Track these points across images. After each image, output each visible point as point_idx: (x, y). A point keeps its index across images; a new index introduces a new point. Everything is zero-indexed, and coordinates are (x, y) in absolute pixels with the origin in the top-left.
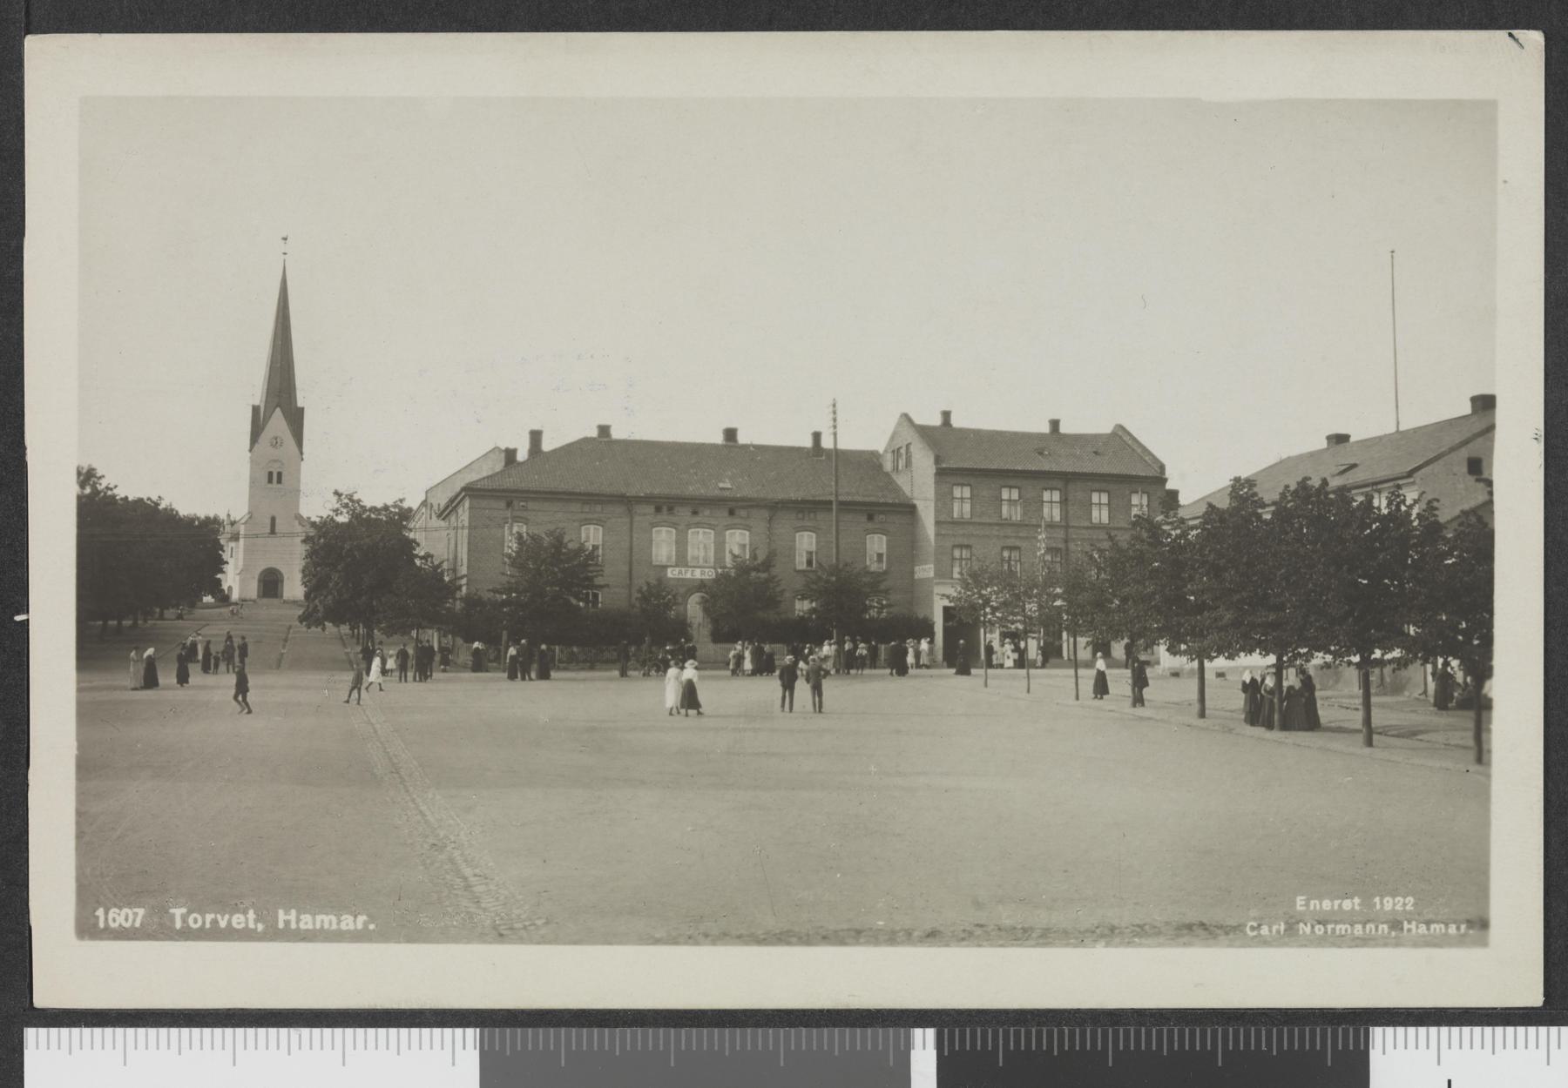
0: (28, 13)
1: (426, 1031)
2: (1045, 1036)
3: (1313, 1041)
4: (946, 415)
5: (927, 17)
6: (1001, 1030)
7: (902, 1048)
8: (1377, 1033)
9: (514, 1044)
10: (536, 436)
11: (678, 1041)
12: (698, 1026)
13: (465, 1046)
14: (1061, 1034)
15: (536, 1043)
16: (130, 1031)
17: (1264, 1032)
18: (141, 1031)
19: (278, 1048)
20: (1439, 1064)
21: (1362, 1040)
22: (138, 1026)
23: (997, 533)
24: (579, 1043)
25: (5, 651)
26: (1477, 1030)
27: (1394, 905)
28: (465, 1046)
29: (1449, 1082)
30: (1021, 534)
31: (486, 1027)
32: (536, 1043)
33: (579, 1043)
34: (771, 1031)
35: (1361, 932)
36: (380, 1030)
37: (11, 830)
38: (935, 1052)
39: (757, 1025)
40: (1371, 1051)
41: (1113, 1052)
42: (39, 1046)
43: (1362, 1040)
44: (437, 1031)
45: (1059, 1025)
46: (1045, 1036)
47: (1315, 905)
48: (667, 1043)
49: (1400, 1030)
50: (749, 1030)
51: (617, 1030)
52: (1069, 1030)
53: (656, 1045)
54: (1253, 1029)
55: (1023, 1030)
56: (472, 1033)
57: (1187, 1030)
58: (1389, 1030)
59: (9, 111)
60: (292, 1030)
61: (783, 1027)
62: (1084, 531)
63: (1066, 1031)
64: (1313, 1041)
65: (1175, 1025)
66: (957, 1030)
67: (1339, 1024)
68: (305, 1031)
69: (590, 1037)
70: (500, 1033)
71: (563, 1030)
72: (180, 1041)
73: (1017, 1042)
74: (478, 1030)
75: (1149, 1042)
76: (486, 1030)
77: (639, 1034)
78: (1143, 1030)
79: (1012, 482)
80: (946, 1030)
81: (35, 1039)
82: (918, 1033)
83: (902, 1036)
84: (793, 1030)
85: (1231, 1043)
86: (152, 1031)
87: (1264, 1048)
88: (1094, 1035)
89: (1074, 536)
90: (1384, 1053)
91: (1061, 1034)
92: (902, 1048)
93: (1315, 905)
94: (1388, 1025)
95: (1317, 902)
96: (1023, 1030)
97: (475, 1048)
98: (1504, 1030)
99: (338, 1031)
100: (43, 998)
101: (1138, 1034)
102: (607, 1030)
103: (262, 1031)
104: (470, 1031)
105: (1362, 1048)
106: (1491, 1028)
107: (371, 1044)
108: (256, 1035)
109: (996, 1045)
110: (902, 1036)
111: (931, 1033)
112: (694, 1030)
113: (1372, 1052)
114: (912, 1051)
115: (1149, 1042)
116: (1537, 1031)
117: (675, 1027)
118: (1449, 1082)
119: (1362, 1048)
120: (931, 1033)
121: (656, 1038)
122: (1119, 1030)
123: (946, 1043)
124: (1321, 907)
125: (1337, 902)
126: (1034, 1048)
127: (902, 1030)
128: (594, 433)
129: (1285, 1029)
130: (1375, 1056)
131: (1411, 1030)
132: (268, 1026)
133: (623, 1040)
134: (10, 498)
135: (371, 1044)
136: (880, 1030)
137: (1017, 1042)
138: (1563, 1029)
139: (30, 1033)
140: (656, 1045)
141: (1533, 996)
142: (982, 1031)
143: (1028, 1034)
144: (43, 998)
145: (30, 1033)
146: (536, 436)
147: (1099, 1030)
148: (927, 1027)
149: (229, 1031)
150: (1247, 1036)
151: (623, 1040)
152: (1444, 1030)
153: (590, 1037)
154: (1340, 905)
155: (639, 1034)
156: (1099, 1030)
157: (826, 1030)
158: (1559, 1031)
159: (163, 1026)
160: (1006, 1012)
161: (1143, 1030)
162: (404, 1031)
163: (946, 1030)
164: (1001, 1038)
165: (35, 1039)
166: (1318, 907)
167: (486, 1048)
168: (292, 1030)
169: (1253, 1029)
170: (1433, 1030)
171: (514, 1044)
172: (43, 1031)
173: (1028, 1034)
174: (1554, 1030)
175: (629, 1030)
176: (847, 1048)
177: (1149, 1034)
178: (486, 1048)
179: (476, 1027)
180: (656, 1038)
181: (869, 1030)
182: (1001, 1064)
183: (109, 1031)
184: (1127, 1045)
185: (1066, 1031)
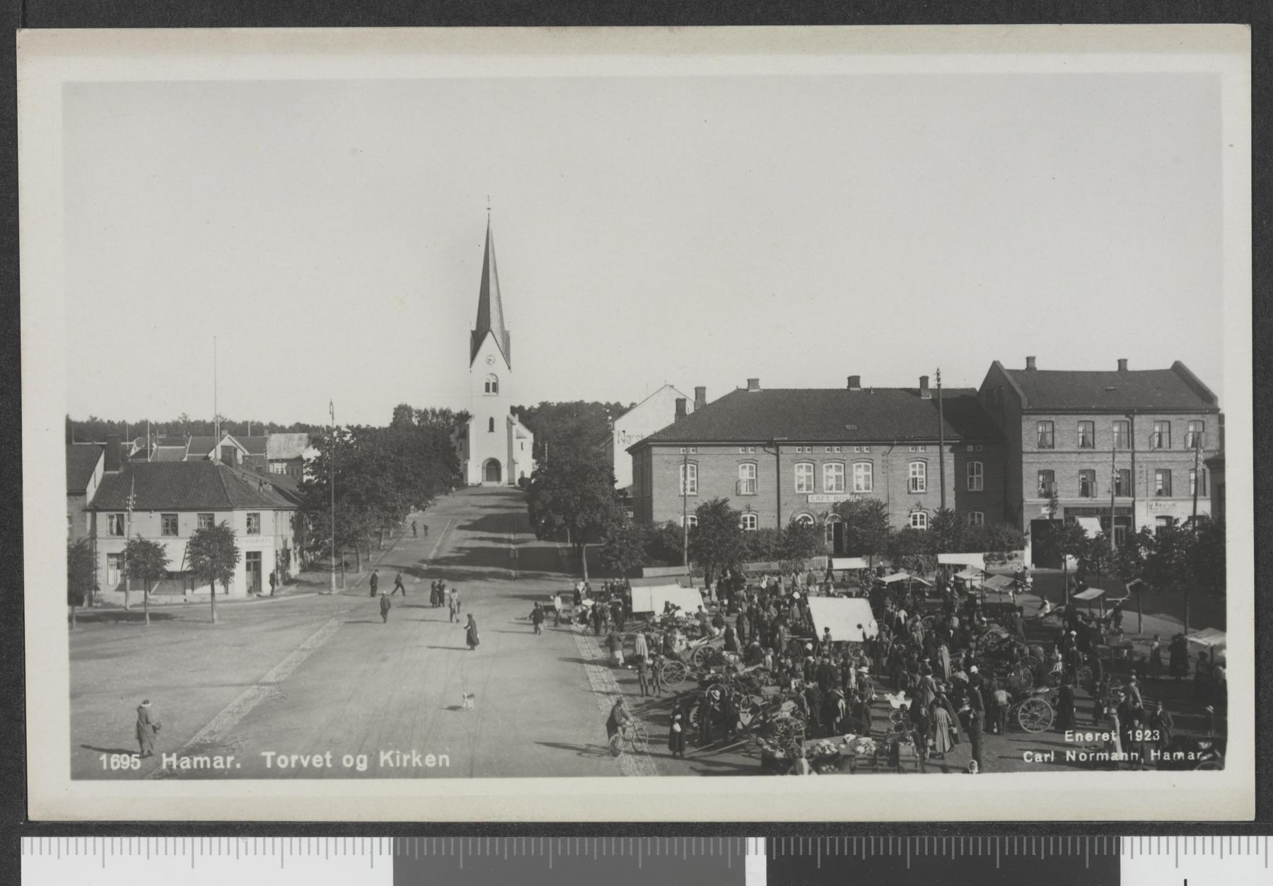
0: (24, 8)
1: (349, 840)
2: (855, 844)
3: (806, 847)
4: (1030, 360)
5: (759, 11)
6: (819, 839)
7: (739, 854)
8: (1126, 841)
9: (600, 851)
10: (700, 392)
11: (466, 847)
12: (572, 836)
13: (382, 851)
14: (868, 842)
15: (663, 850)
16: (108, 840)
17: (1034, 841)
18: (117, 839)
19: (50, 853)
20: (104, 867)
21: (399, 847)
22: (115, 836)
23: (1074, 460)
24: (475, 849)
25: (5, 529)
26: (1208, 839)
27: (1144, 736)
28: (382, 851)
29: (1186, 881)
30: (1095, 460)
31: (398, 836)
32: (663, 850)
33: (475, 849)
34: (631, 839)
35: (1169, 759)
36: (34, 838)
37: (11, 675)
38: (765, 856)
39: (620, 835)
40: (1122, 856)
41: (911, 857)
42: (34, 852)
43: (399, 847)
44: (358, 840)
45: (866, 834)
46: (855, 844)
47: (1079, 738)
48: (546, 850)
49: (1145, 839)
50: (613, 839)
51: (506, 839)
52: (875, 839)
53: (537, 851)
54: (1025, 838)
55: (837, 838)
56: (387, 842)
57: (971, 839)
58: (1137, 839)
59: (8, 87)
60: (240, 839)
61: (641, 836)
62: (1148, 455)
63: (873, 840)
64: (806, 847)
65: (961, 835)
66: (783, 839)
67: (1095, 834)
68: (251, 840)
69: (573, 845)
70: (696, 841)
71: (461, 839)
72: (166, 847)
73: (832, 849)
74: (392, 839)
75: (940, 849)
76: (399, 839)
77: (524, 843)
78: (935, 839)
79: (1044, 418)
80: (774, 839)
81: (29, 844)
82: (751, 841)
83: (739, 843)
84: (649, 839)
85: (1007, 849)
86: (126, 840)
87: (1034, 854)
88: (895, 842)
89: (1140, 460)
90: (1132, 857)
91: (868, 842)
92: (739, 854)
93: (1079, 738)
94: (1136, 835)
95: (1081, 735)
96: (837, 838)
97: (390, 854)
98: (1150, 839)
99: (278, 840)
100: (35, 814)
101: (931, 841)
102: (497, 839)
103: (215, 840)
104: (385, 840)
105: (1114, 853)
106: (1219, 837)
107: (170, 850)
108: (130, 842)
109: (815, 851)
110: (739, 843)
111: (762, 841)
112: (569, 839)
113: (1122, 857)
114: (747, 856)
115: (850, 849)
116: (1150, 839)
117: (552, 836)
118: (1186, 881)
119: (1114, 853)
120: (762, 841)
121: (537, 846)
122: (915, 839)
123: (774, 849)
124: (1084, 738)
125: (1097, 735)
126: (891, 854)
127: (739, 839)
128: (744, 385)
129: (1052, 838)
130: (1125, 860)
131: (1154, 839)
132: (220, 836)
133: (510, 847)
134: (10, 404)
135: (170, 850)
136: (721, 839)
137: (832, 849)
138: (1271, 838)
139: (26, 842)
140: (537, 851)
141: (1247, 812)
142: (1063, 839)
143: (841, 842)
144: (35, 814)
145: (26, 842)
146: (700, 392)
147: (900, 839)
148: (759, 836)
149: (188, 840)
150: (1083, 844)
151: (510, 847)
152: (1181, 839)
153: (573, 845)
154: (1100, 737)
155: (524, 843)
156: (900, 839)
157: (676, 839)
158: (1204, 839)
159: (170, 835)
160: (824, 824)
161: (935, 839)
162: (331, 840)
163: (774, 839)
164: (819, 845)
165: (29, 844)
166: (1082, 740)
167: (399, 854)
168: (240, 839)
169: (1025, 838)
170: (1172, 839)
171: (600, 851)
172: (36, 840)
173: (841, 842)
174: (1262, 838)
175: (515, 839)
176: (443, 854)
177: (940, 842)
178: (399, 854)
179: (390, 835)
180: (537, 846)
181: (711, 839)
182: (819, 867)
183: (90, 839)
184: (1101, 850)
185: (873, 840)
